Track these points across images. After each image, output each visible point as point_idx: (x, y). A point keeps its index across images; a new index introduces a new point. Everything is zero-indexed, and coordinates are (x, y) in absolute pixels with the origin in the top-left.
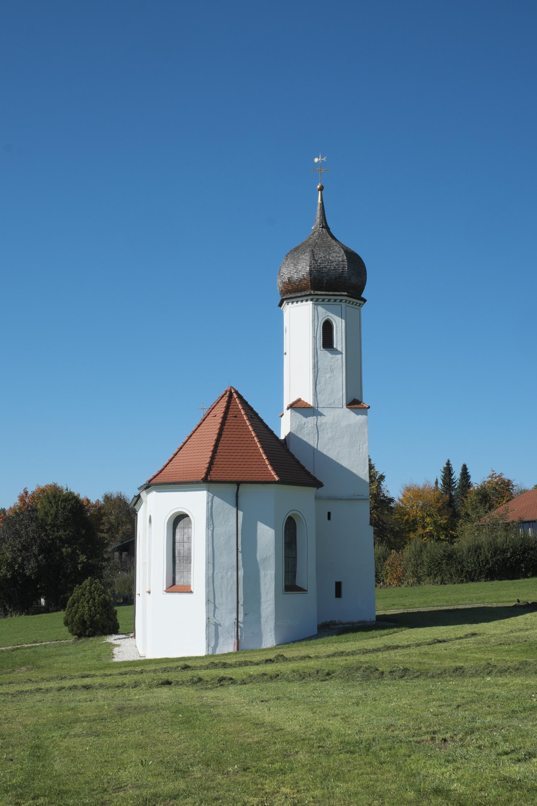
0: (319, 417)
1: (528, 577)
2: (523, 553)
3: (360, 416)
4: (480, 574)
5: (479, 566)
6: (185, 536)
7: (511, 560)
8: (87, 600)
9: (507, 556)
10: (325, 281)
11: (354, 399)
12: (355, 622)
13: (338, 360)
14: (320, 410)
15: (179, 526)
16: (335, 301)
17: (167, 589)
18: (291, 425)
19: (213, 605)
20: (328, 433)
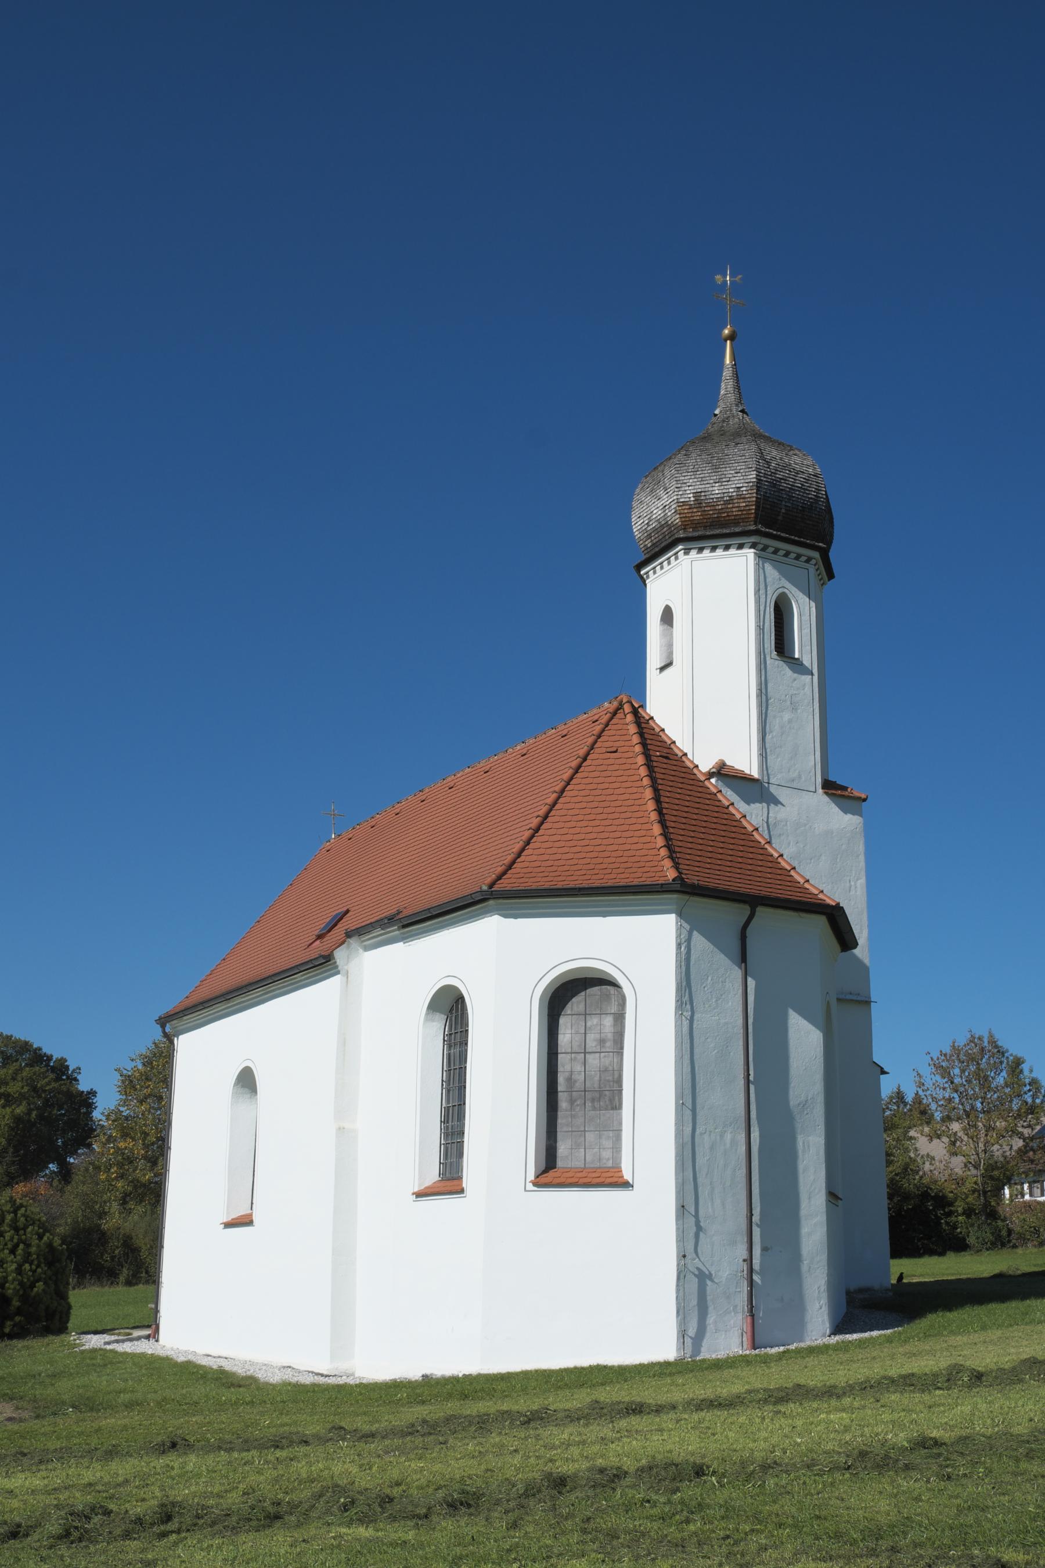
3: (849, 816)
6: (591, 1037)
8: (9, 1246)
13: (804, 685)
14: (773, 789)
15: (568, 1009)
17: (537, 1177)
20: (789, 844)
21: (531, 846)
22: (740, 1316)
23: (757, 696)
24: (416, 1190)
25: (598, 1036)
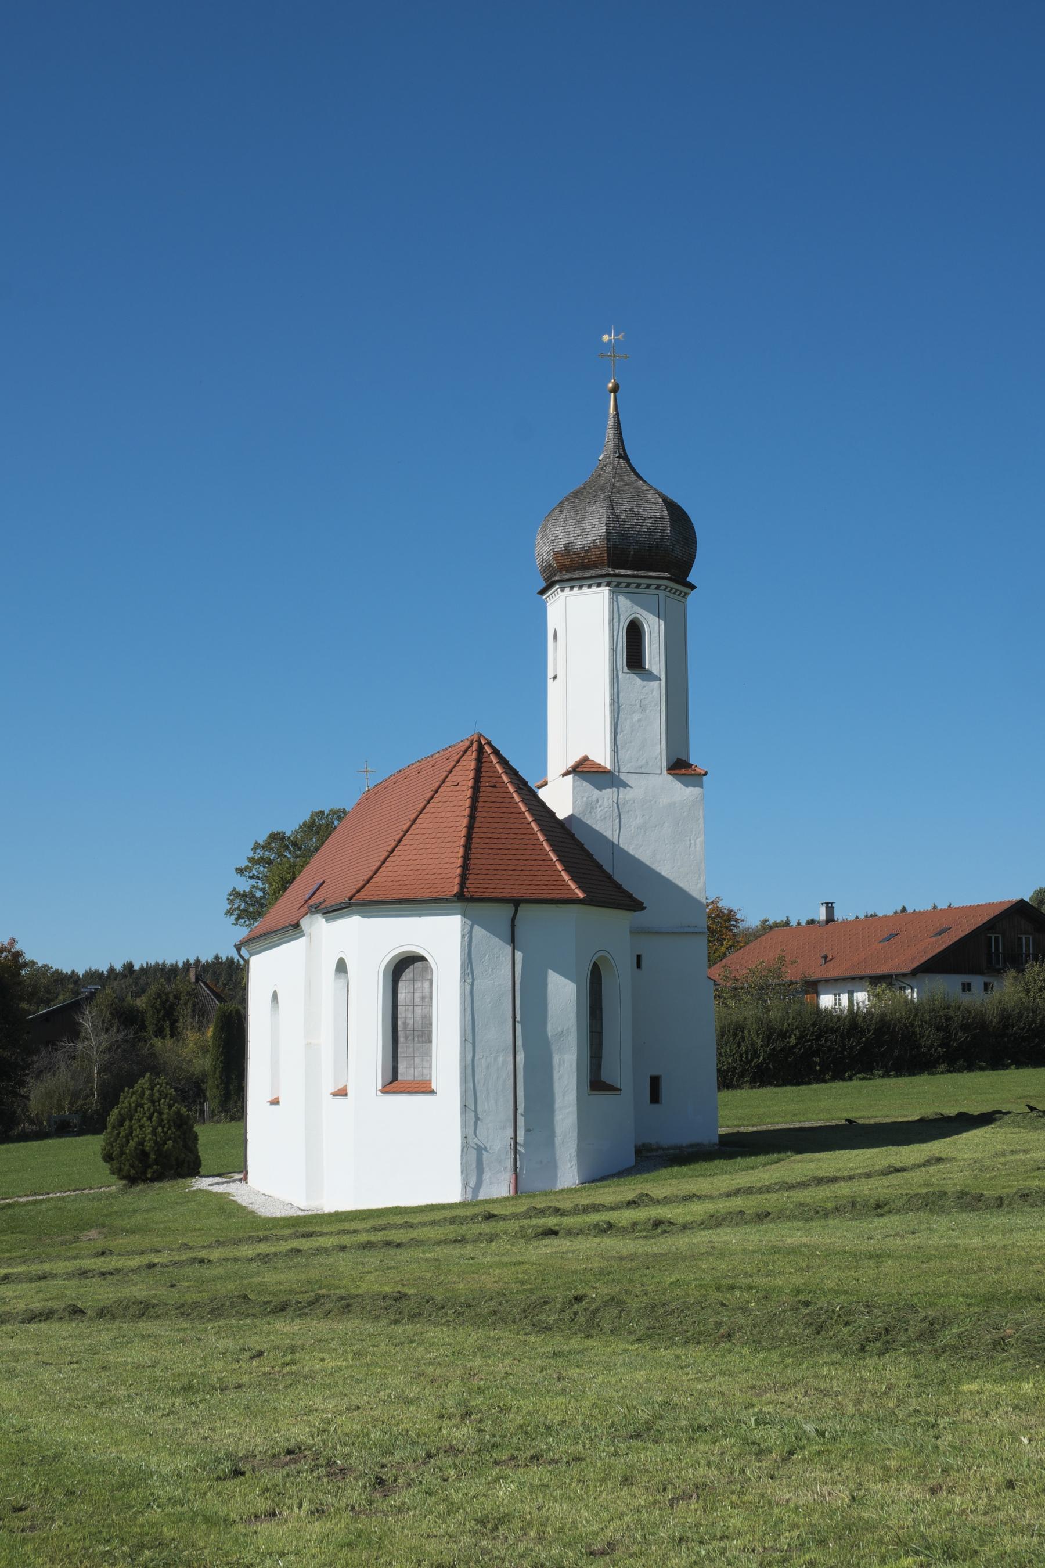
0: (621, 789)
1: (825, 1081)
2: (819, 1038)
3: (691, 789)
4: (742, 1076)
5: (741, 1060)
6: (417, 995)
7: (797, 1051)
8: (147, 1115)
9: (789, 1042)
10: (632, 553)
11: (678, 759)
12: (684, 1145)
14: (623, 777)
15: (404, 977)
16: (648, 586)
17: (384, 1087)
18: (575, 802)
19: (473, 1114)
20: (636, 817)
21: (386, 865)
22: (508, 1174)
23: (610, 705)
24: (332, 1091)
25: (421, 995)
